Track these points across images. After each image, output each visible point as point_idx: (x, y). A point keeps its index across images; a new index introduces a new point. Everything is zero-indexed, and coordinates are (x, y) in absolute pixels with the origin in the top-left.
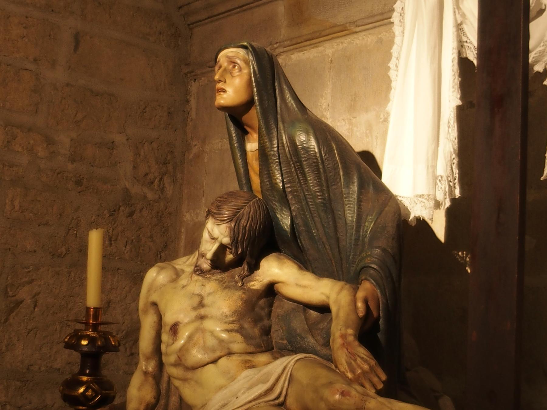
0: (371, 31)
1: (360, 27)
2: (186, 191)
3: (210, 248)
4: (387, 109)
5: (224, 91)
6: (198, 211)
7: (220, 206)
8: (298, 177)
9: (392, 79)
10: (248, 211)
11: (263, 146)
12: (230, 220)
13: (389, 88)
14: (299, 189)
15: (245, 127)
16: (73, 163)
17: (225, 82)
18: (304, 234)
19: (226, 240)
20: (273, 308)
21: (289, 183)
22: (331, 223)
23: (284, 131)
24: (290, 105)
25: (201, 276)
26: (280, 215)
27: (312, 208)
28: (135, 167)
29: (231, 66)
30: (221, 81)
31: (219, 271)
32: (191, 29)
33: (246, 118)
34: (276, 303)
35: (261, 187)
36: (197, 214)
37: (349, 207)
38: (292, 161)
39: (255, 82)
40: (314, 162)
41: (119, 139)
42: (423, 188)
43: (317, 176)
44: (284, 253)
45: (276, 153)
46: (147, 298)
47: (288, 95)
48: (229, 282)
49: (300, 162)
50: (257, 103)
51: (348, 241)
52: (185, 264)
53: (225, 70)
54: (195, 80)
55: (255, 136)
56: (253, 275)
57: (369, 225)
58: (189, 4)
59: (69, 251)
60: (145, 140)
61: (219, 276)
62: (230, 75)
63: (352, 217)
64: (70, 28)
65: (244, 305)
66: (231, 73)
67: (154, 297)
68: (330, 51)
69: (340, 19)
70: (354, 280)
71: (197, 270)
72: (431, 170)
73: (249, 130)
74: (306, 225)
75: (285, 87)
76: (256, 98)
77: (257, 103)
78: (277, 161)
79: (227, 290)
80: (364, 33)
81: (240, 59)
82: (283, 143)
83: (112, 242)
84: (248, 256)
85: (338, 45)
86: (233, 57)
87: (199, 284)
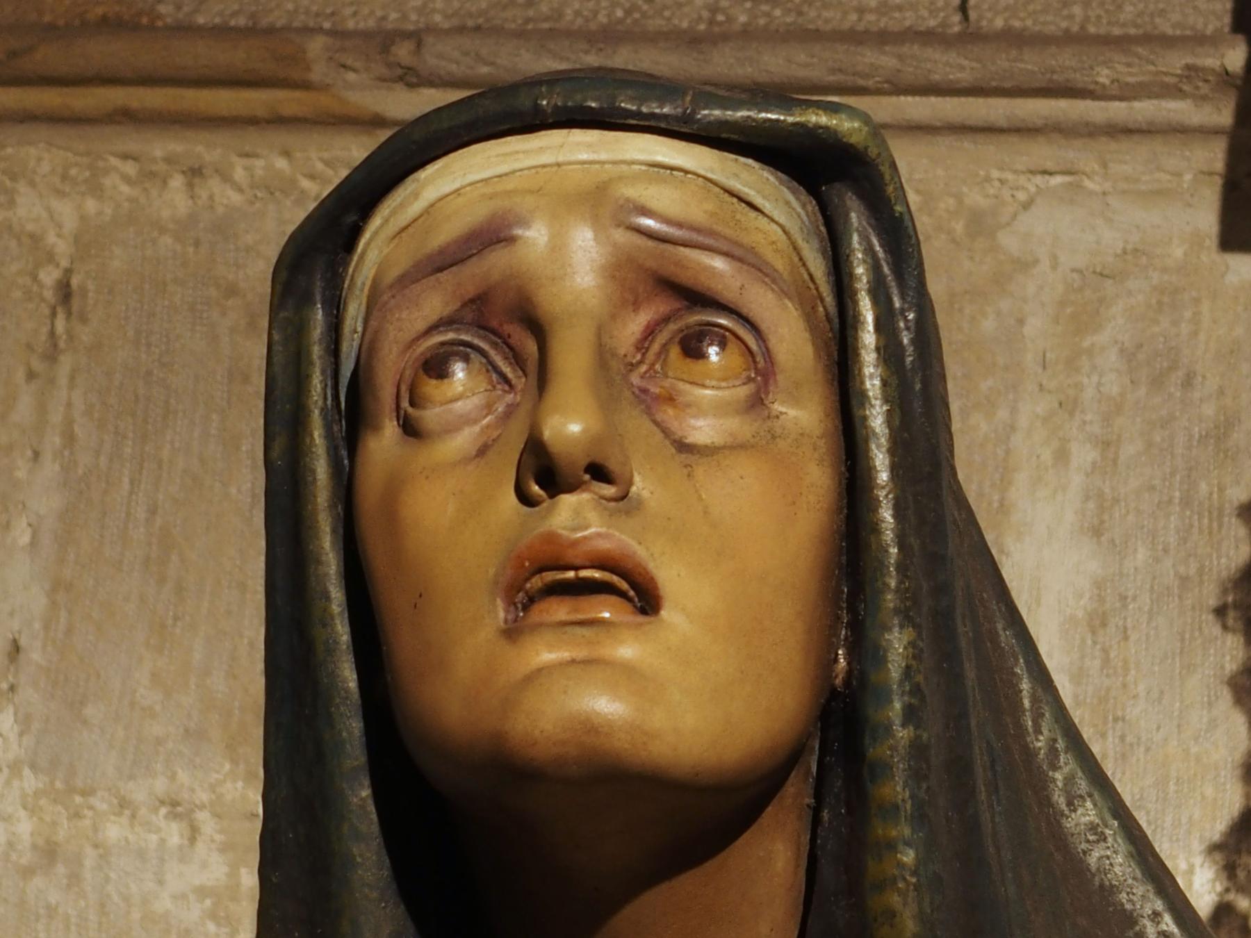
68: (66, 211)
85: (150, 177)
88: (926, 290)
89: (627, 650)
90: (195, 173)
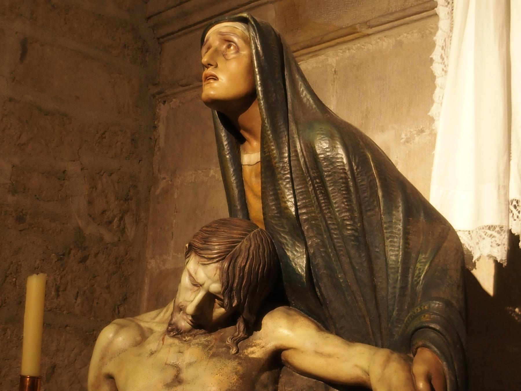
0: (387, 33)
1: (373, 29)
2: (151, 233)
3: (192, 299)
4: (429, 114)
5: (216, 78)
6: (165, 257)
7: (208, 238)
8: (318, 199)
9: (436, 74)
10: (247, 246)
11: (269, 156)
12: (222, 258)
13: (433, 87)
14: (320, 215)
15: (242, 132)
16: (13, 195)
17: (216, 66)
18: (325, 280)
19: (215, 287)
20: (279, 385)
21: (305, 207)
22: (365, 264)
23: (298, 133)
24: (305, 100)
25: (178, 338)
26: (292, 252)
27: (339, 243)
28: (90, 203)
29: (224, 47)
30: (211, 65)
31: (203, 331)
32: (161, 44)
33: (243, 118)
34: (283, 379)
35: (264, 214)
36: (164, 261)
37: (391, 242)
38: (310, 176)
39: (258, 66)
40: (342, 178)
41: (72, 168)
42: (492, 216)
43: (345, 198)
44: (295, 307)
45: (287, 165)
46: (100, 368)
47: (302, 88)
48: (218, 347)
49: (321, 177)
50: (261, 95)
51: (390, 290)
52: (154, 321)
53: (216, 51)
54: (165, 102)
55: (256, 144)
56: (251, 338)
57: (422, 267)
58: (160, 13)
59: (5, 303)
60: (103, 172)
61: (203, 339)
62: (223, 58)
63: (396, 255)
64: (16, 33)
65: (241, 381)
66: (224, 56)
67: (110, 368)
68: (334, 60)
69: (347, 21)
70: (404, 347)
71: (172, 330)
72: (502, 192)
73: (246, 135)
74: (329, 267)
75: (297, 77)
76: (259, 89)
77: (261, 95)
78: (289, 176)
79: (215, 359)
80: (378, 36)
81: (238, 36)
82: (296, 151)
83: (60, 293)
84: (246, 311)
85: (344, 52)
86: (227, 33)
87: (174, 349)
88: (102, 329)
90: (349, 49)
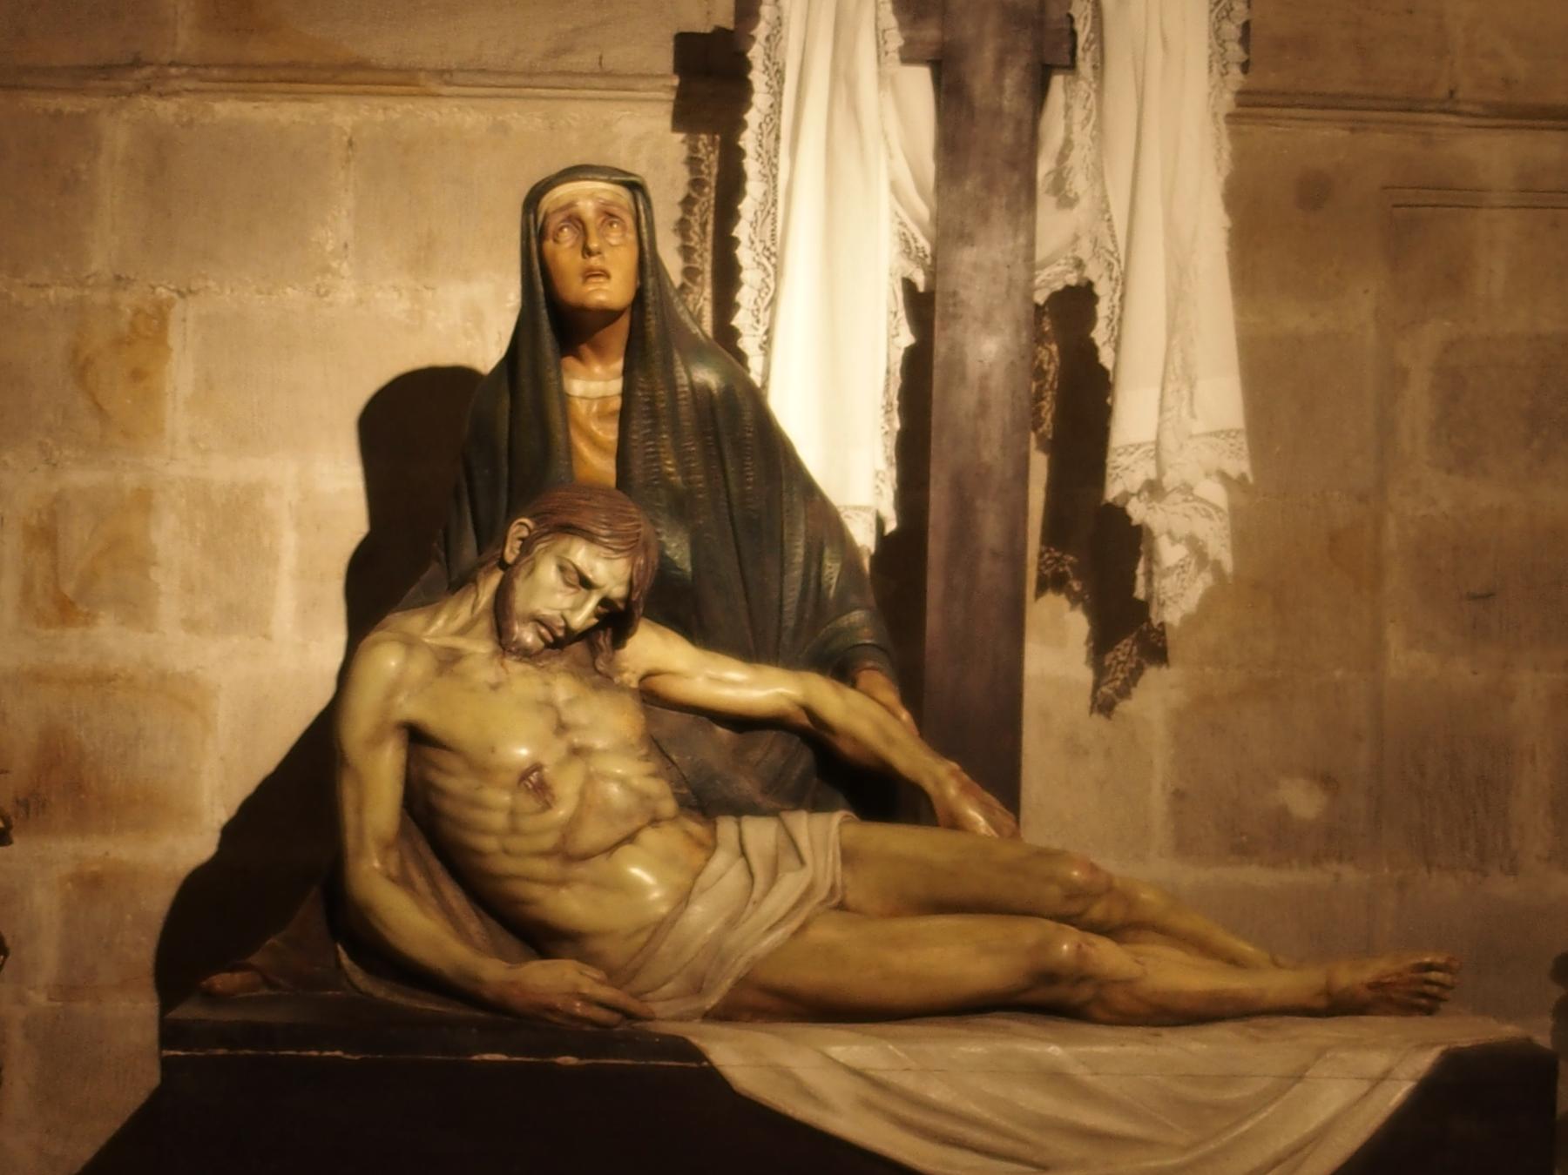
0: (477, 102)
69: (382, 48)
80: (457, 102)
89: (606, 287)
